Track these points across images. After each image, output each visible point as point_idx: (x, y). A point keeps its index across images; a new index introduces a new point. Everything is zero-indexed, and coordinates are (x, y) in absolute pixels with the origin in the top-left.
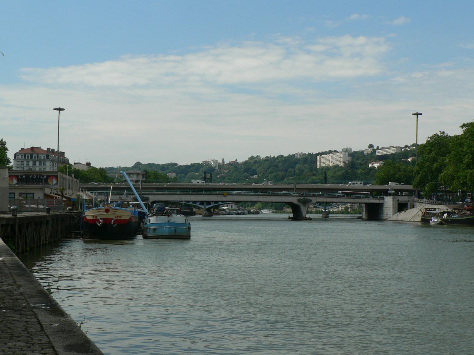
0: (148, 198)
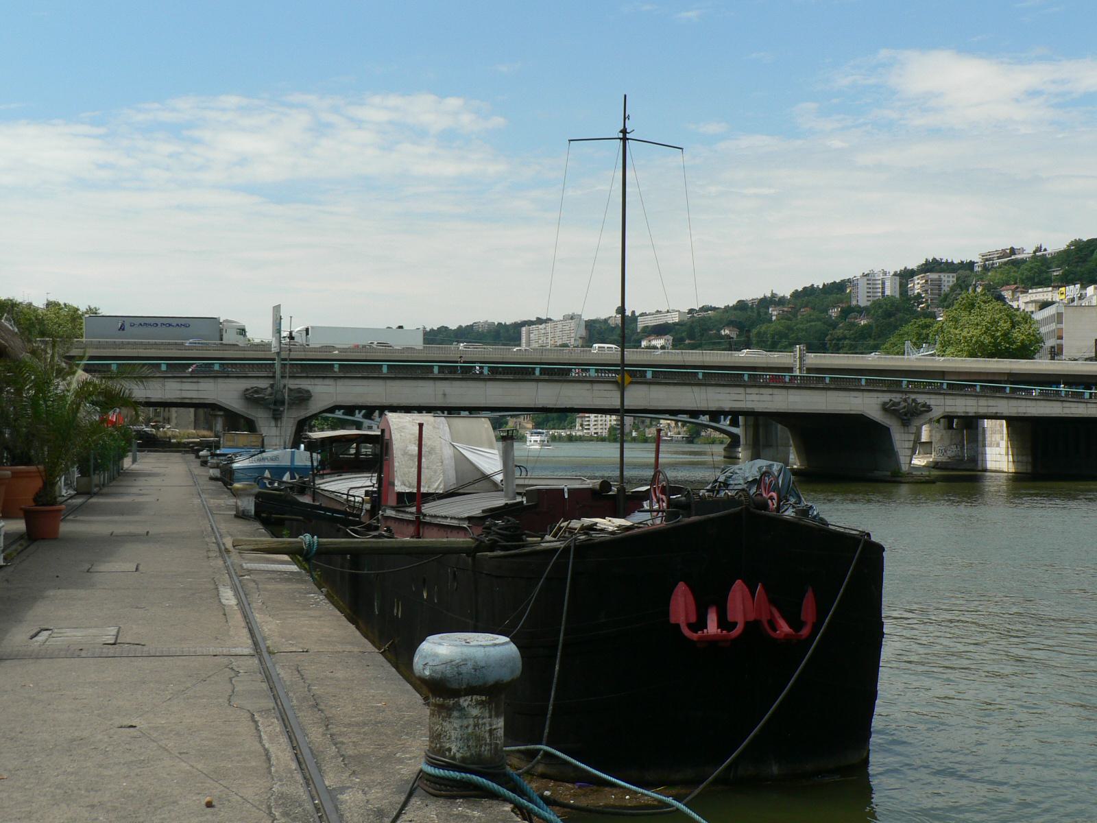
0: (308, 391)
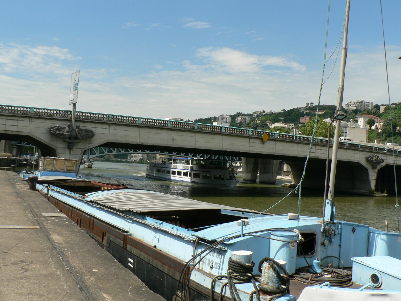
0: (92, 132)
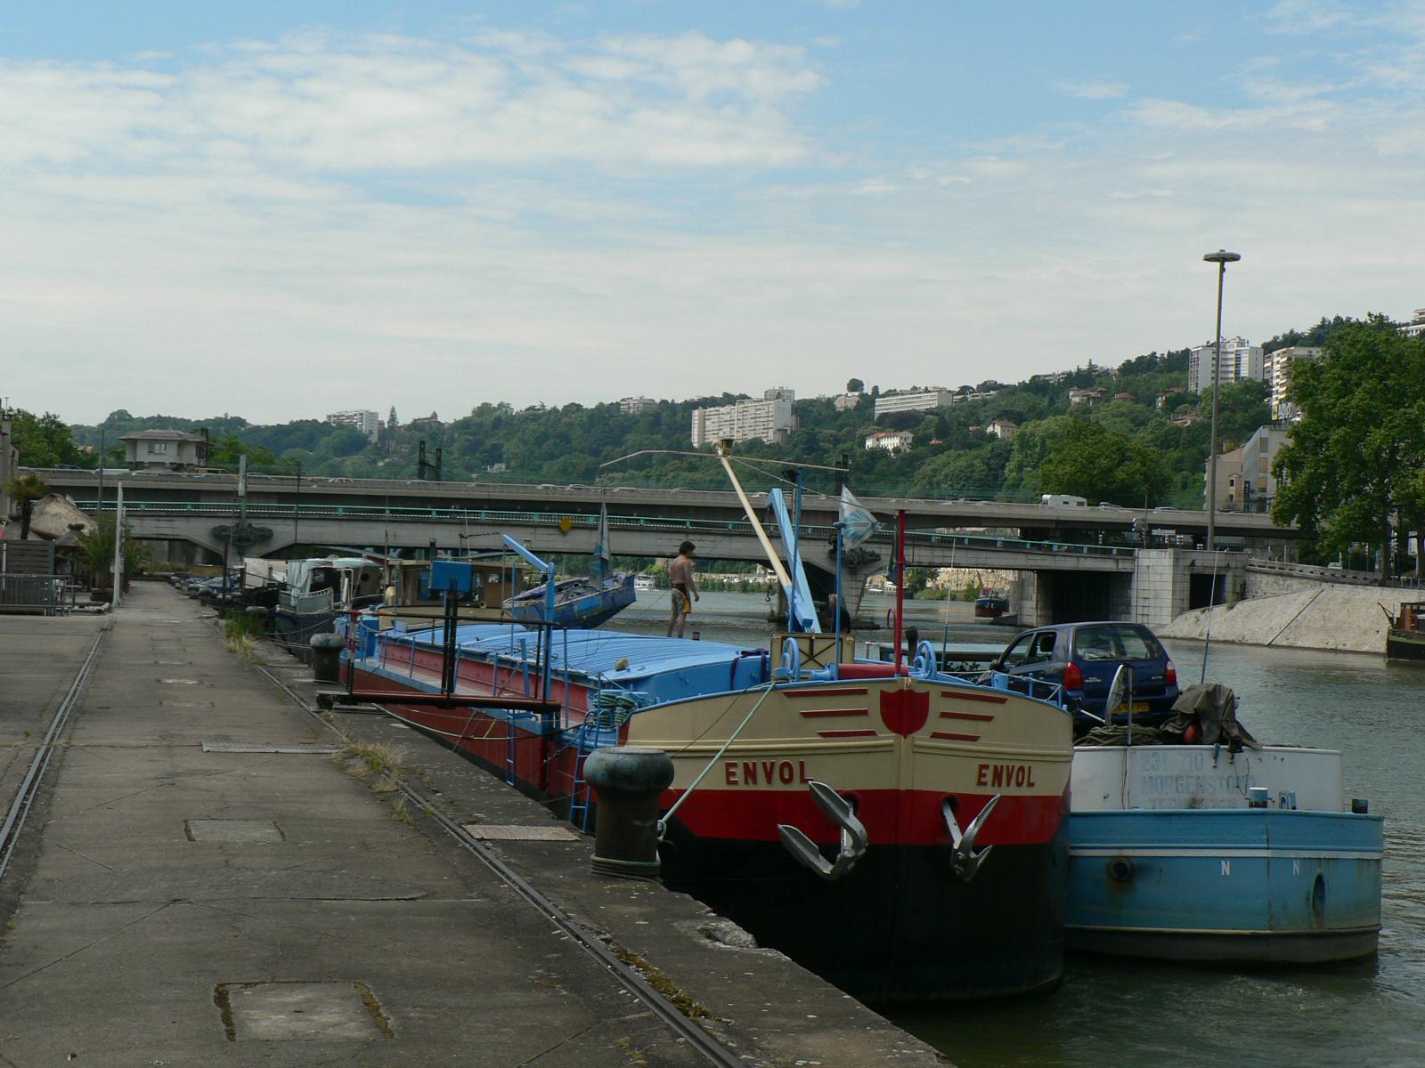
0: (270, 530)
